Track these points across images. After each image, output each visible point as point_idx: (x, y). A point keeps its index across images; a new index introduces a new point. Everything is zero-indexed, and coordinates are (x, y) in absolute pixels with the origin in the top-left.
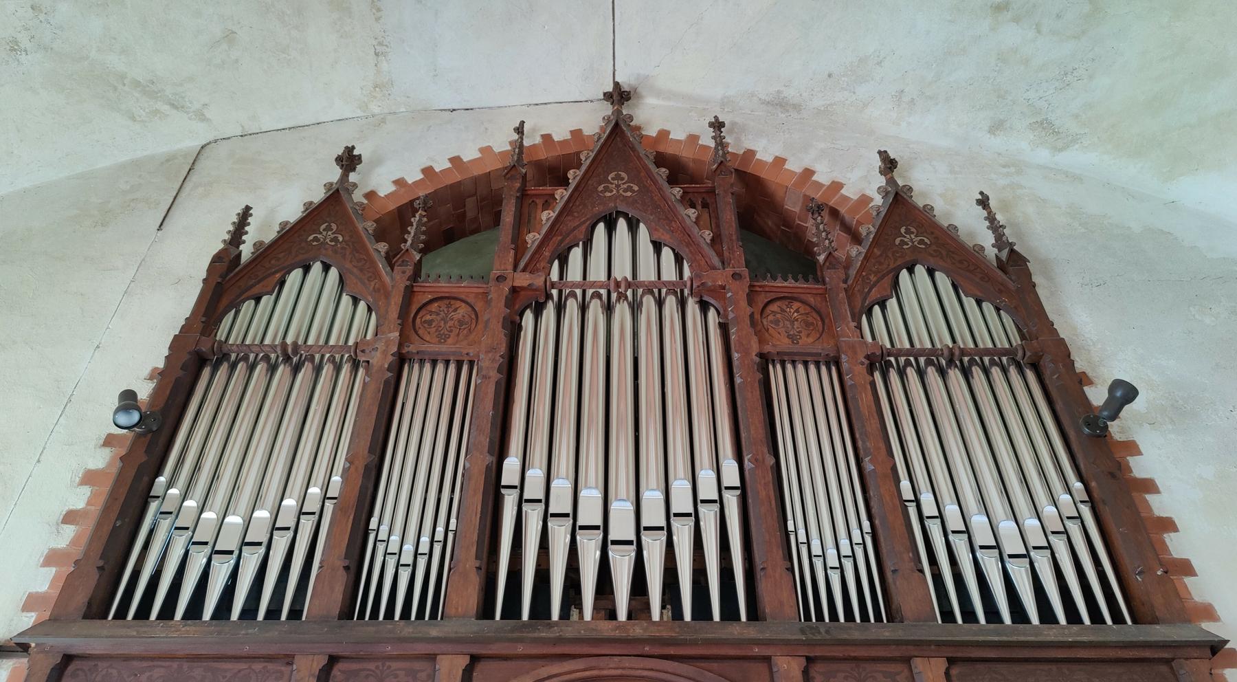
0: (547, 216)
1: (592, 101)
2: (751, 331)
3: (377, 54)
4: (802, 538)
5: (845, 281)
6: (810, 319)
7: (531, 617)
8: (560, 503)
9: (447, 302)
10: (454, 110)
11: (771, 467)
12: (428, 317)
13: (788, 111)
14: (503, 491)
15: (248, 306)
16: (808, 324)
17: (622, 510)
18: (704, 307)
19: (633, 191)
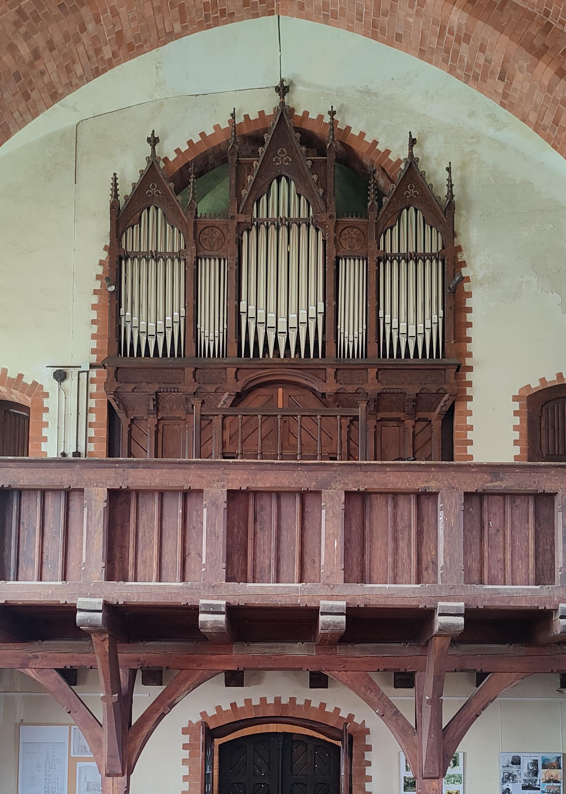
0: (250, 178)
1: (269, 88)
2: (334, 246)
3: (157, 68)
4: (342, 331)
5: (376, 219)
6: (360, 237)
7: (253, 357)
8: (261, 319)
9: (211, 228)
10: (197, 95)
11: (334, 306)
12: (204, 237)
13: (371, 97)
14: (241, 314)
15: (129, 231)
16: (358, 240)
17: (282, 321)
18: (317, 230)
19: (289, 162)
